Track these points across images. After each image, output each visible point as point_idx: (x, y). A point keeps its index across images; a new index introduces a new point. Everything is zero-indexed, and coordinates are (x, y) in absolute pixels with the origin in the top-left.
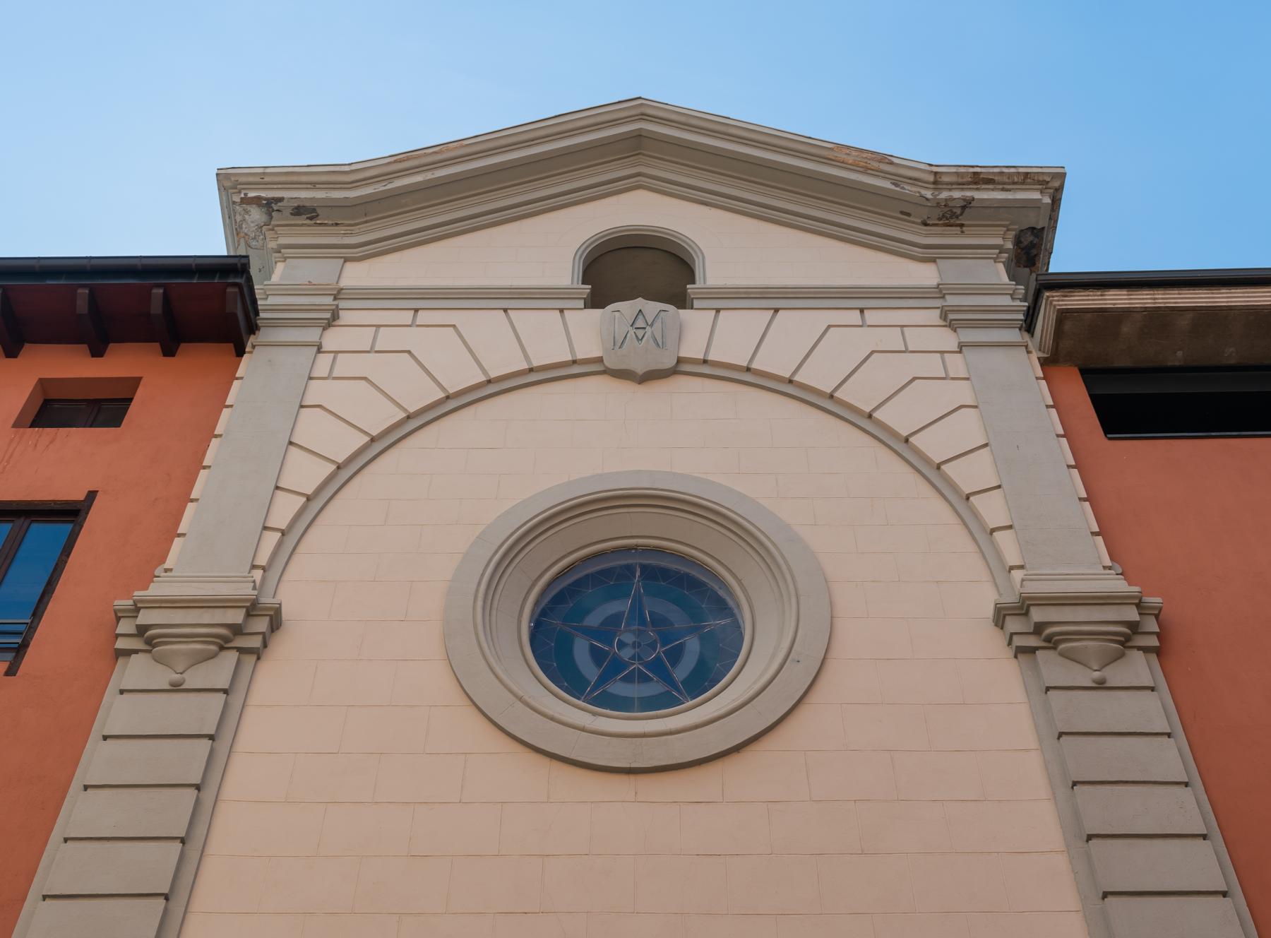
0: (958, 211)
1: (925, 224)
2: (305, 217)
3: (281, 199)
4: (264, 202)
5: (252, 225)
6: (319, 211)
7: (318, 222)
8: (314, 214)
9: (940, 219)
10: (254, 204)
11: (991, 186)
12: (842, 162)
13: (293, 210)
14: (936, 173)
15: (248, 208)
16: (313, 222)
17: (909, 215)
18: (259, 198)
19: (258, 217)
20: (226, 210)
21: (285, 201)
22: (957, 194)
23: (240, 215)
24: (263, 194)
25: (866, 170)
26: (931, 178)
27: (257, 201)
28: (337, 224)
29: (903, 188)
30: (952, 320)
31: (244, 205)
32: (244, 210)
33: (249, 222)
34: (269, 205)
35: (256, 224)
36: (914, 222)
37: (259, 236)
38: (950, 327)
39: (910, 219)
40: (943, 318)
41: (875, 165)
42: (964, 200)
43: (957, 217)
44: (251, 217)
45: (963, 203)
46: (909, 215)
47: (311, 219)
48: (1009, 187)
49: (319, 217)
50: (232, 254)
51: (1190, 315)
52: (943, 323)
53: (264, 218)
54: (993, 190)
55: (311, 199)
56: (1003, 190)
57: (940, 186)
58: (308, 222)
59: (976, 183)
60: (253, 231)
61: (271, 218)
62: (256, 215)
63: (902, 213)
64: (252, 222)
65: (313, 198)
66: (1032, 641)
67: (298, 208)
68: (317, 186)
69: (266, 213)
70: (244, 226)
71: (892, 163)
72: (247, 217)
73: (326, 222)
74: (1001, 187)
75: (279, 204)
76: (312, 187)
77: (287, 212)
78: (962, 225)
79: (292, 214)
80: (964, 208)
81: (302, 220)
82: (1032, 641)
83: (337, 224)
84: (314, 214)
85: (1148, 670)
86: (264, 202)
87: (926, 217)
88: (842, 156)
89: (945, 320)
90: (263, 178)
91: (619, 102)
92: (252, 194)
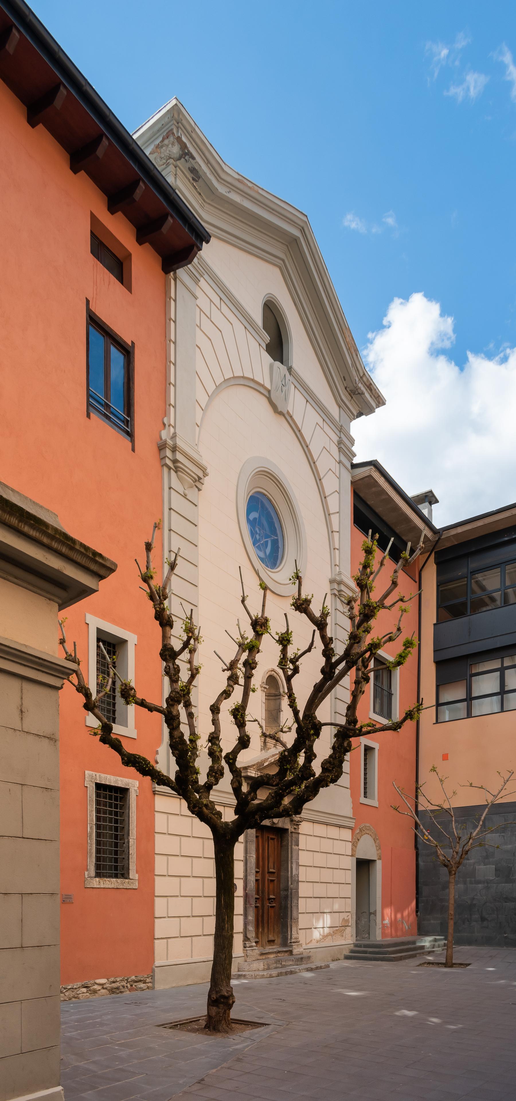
0: (357, 393)
1: (346, 388)
2: (192, 175)
3: (194, 158)
4: (186, 151)
5: (168, 152)
6: (201, 180)
7: (194, 184)
8: (197, 179)
9: (350, 390)
10: (181, 145)
11: (369, 392)
12: (345, 338)
13: (192, 167)
14: (364, 374)
15: (176, 143)
16: (192, 181)
17: (345, 380)
18: (186, 146)
19: (175, 152)
20: (160, 125)
21: (195, 161)
22: (363, 388)
23: (169, 142)
24: (189, 145)
25: (349, 349)
26: (362, 375)
27: (183, 146)
28: (200, 194)
29: (352, 367)
30: (341, 447)
31: (176, 140)
32: (173, 142)
33: (168, 149)
34: (185, 154)
35: (170, 153)
36: (344, 384)
37: (164, 159)
38: (339, 448)
39: (344, 382)
40: (339, 442)
41: (353, 351)
42: (362, 392)
43: (354, 394)
44: (173, 148)
45: (361, 392)
46: (345, 380)
47: (193, 179)
48: (372, 396)
49: (197, 182)
50: (139, 143)
51: (387, 497)
52: (336, 443)
53: (177, 156)
54: (369, 393)
55: (205, 173)
56: (371, 396)
57: (361, 380)
58: (191, 179)
59: (368, 387)
60: (165, 155)
61: (179, 159)
62: (176, 150)
63: (344, 377)
64: (170, 151)
65: (205, 173)
66: (337, 593)
67: (194, 169)
68: (209, 165)
69: (180, 155)
70: (164, 148)
71: (357, 355)
72: (170, 146)
73: (197, 188)
74: (371, 394)
75: (191, 159)
76: (207, 162)
77: (188, 165)
78: (352, 398)
79: (189, 168)
80: (359, 393)
81: (189, 176)
82: (337, 593)
83: (200, 194)
84: (197, 179)
85: (480, 676)
86: (186, 151)
87: (348, 387)
88: (347, 335)
89: (339, 444)
90: (192, 132)
91: (302, 213)
92: (184, 139)
